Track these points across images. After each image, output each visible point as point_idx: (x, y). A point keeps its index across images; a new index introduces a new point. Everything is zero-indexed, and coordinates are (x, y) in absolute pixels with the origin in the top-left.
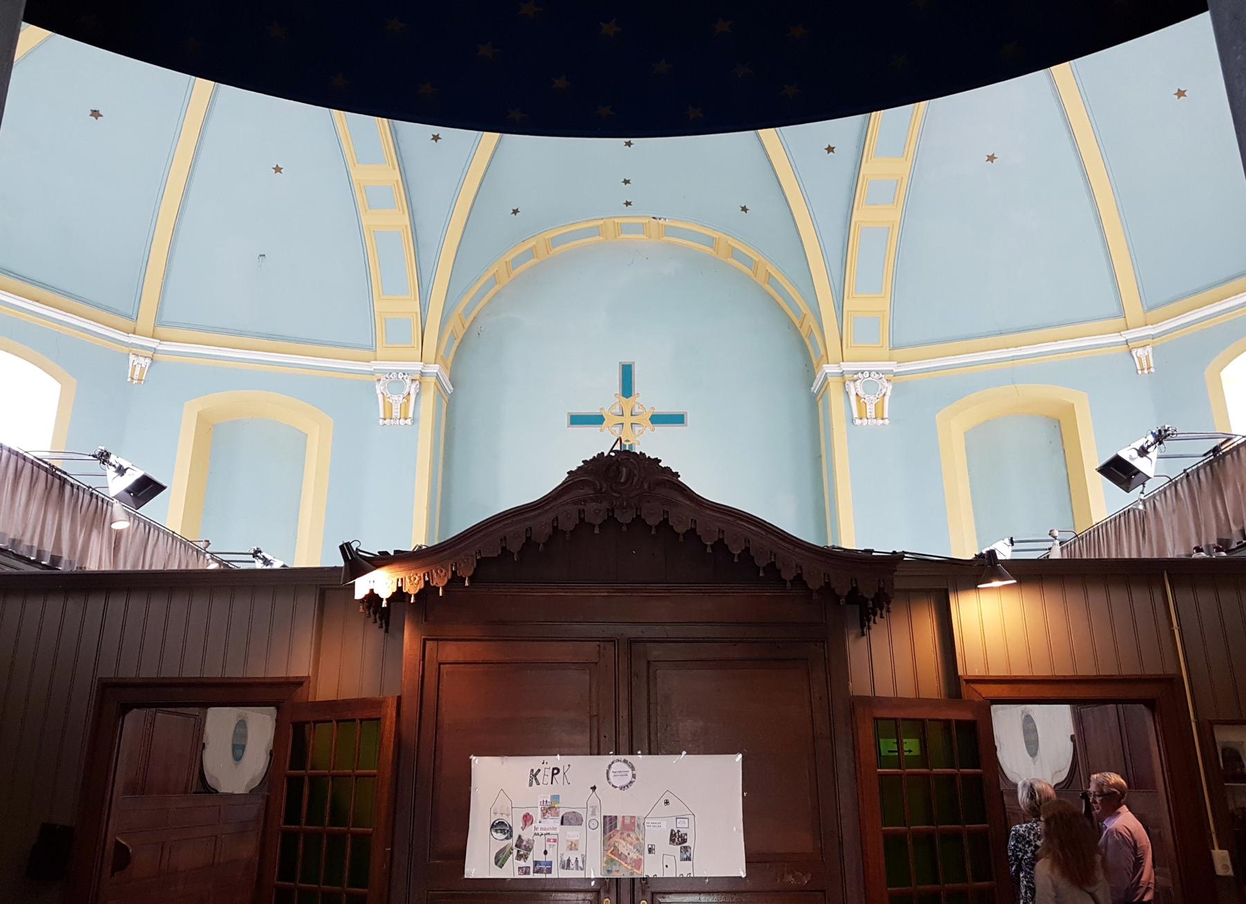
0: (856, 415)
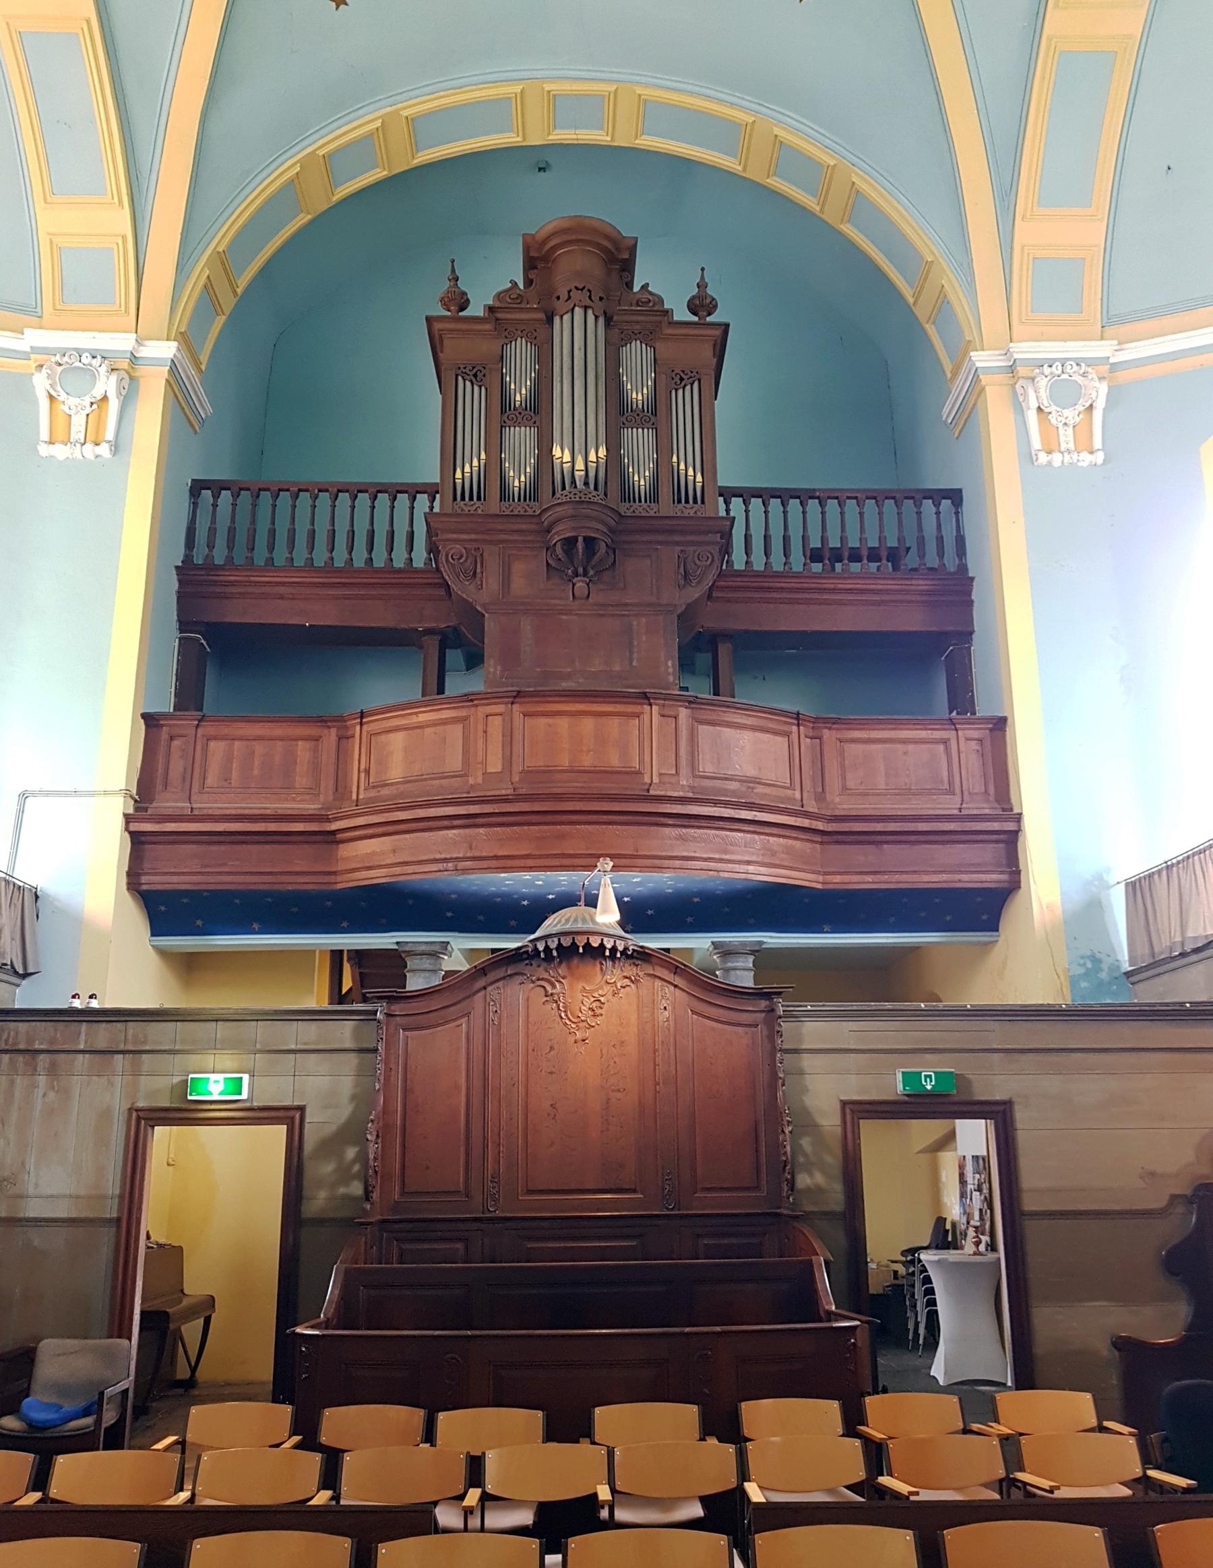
0: (1036, 443)
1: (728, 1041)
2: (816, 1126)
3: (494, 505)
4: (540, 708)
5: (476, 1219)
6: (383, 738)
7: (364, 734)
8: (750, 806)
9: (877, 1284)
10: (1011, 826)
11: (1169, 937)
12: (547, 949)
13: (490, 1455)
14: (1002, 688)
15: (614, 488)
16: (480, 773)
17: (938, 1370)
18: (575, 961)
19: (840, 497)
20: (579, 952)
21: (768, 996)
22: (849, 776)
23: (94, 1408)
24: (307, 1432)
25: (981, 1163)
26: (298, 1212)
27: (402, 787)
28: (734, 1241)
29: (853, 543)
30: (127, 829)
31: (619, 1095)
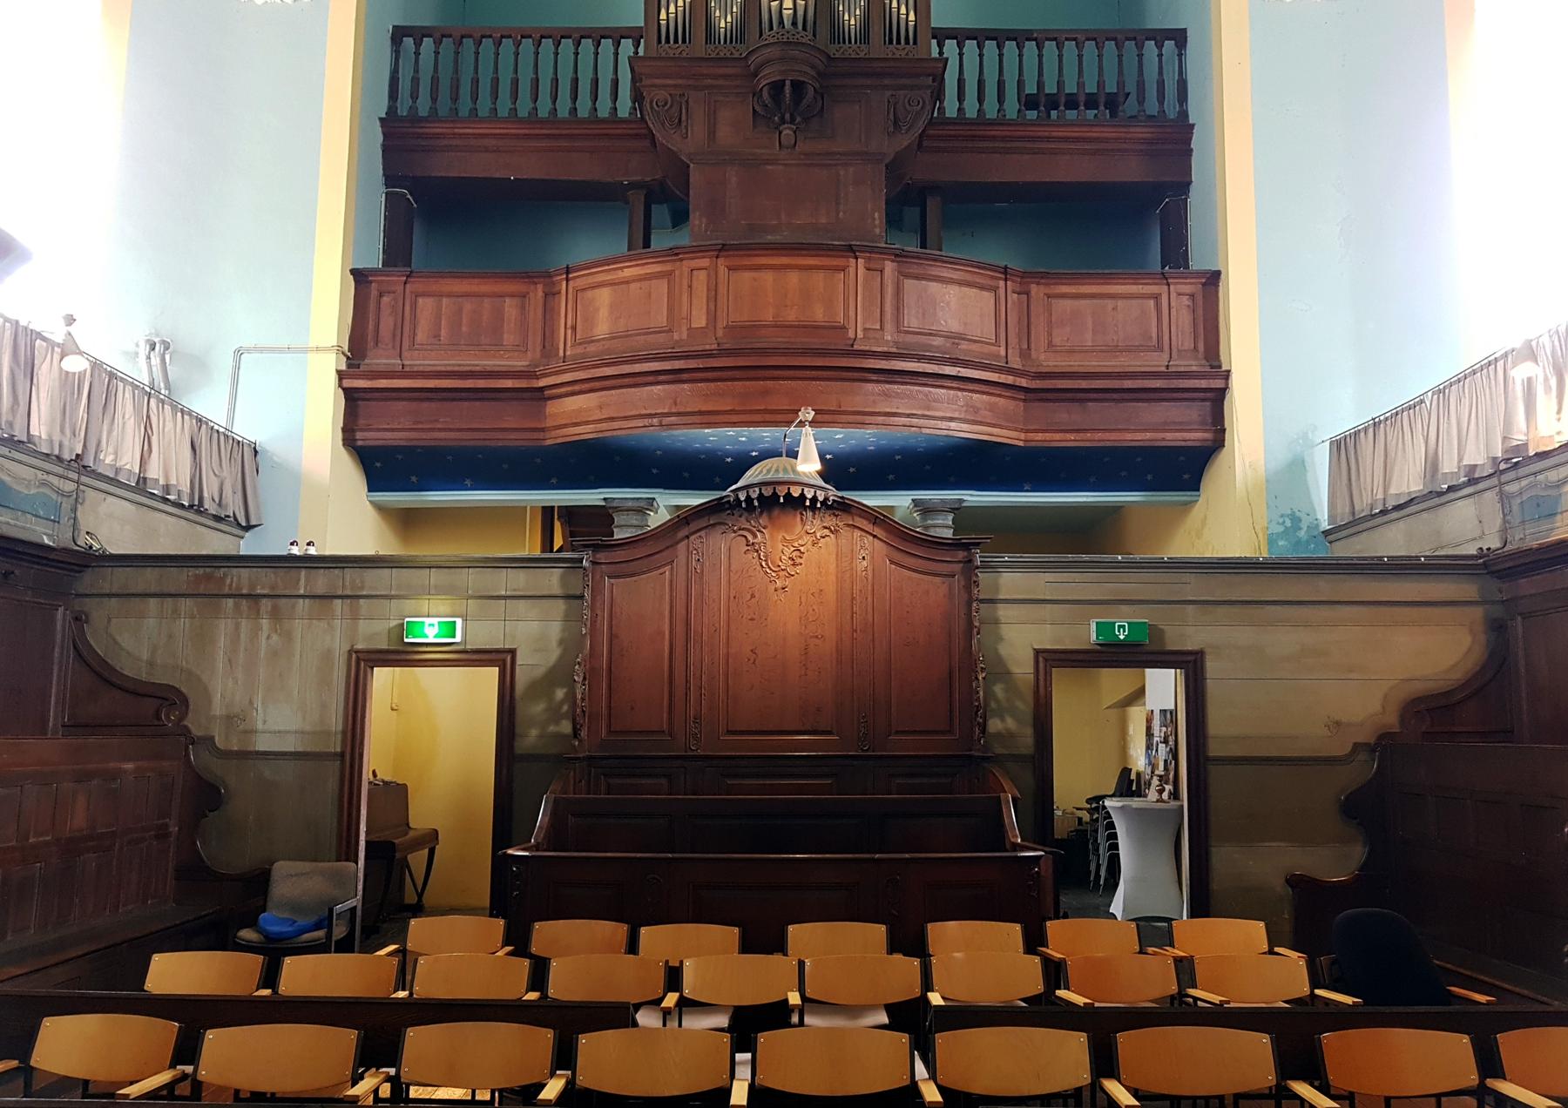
1: (926, 592)
2: (1009, 673)
3: (699, 47)
4: (747, 262)
5: (677, 757)
6: (589, 294)
8: (955, 362)
9: (1061, 830)
10: (1219, 384)
11: (1371, 494)
12: (749, 499)
13: (687, 963)
14: (1217, 242)
15: (824, 31)
16: (684, 329)
17: (1117, 907)
18: (776, 512)
19: (1058, 38)
20: (780, 503)
21: (967, 547)
22: (1055, 332)
23: (326, 922)
24: (518, 940)
25: (1169, 717)
26: (511, 747)
27: (608, 344)
28: (925, 780)
29: (1071, 87)
30: (340, 386)
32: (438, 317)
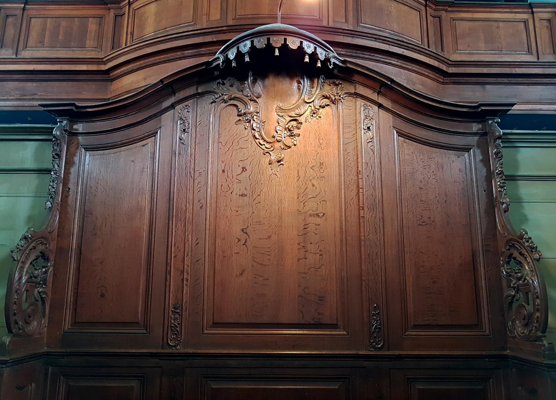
7: (131, 9)
31: (318, 220)
32: (44, 30)
